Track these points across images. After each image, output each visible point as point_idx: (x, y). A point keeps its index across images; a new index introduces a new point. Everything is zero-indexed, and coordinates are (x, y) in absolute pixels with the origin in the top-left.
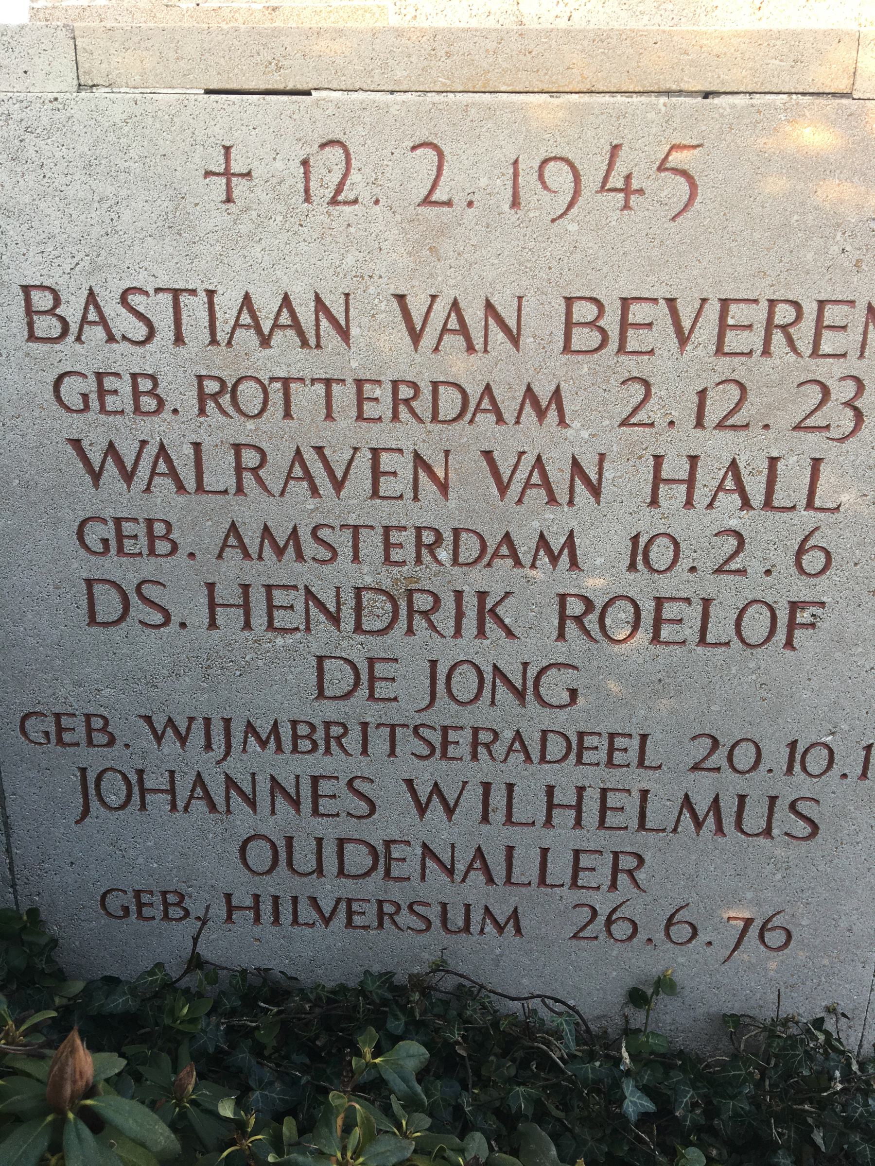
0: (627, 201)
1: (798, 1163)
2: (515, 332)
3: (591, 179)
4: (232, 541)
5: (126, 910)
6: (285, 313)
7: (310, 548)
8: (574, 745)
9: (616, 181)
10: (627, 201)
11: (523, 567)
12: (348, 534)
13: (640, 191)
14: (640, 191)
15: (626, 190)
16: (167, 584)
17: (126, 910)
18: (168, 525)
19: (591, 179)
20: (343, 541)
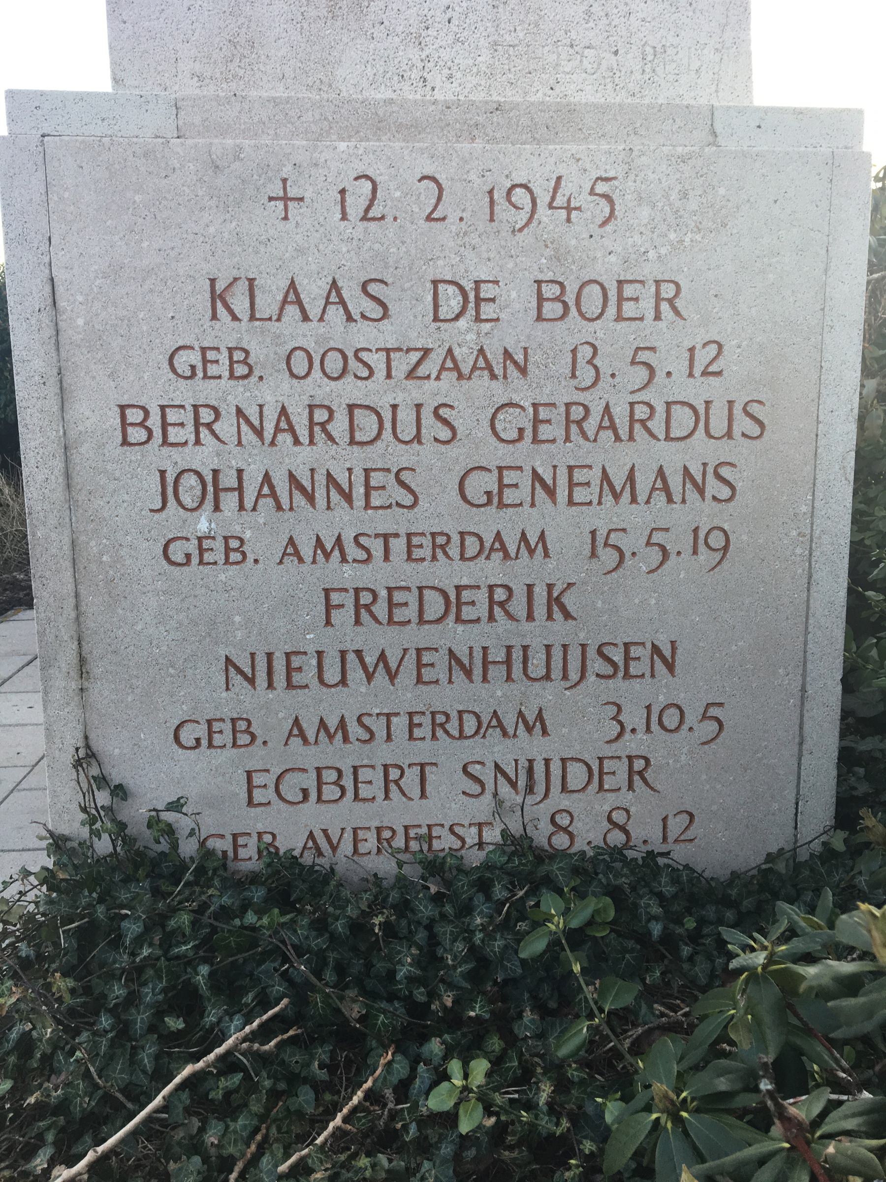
0: (576, 209)
1: (885, 892)
2: (453, 662)
3: (543, 199)
4: (290, 550)
5: (305, 792)
6: (481, 359)
7: (353, 552)
8: (472, 296)
9: (560, 201)
10: (576, 209)
11: (738, 955)
12: (380, 541)
13: (578, 209)
14: (578, 209)
15: (569, 209)
16: (456, 404)
17: (305, 792)
18: (242, 540)
19: (543, 199)
20: (377, 548)
